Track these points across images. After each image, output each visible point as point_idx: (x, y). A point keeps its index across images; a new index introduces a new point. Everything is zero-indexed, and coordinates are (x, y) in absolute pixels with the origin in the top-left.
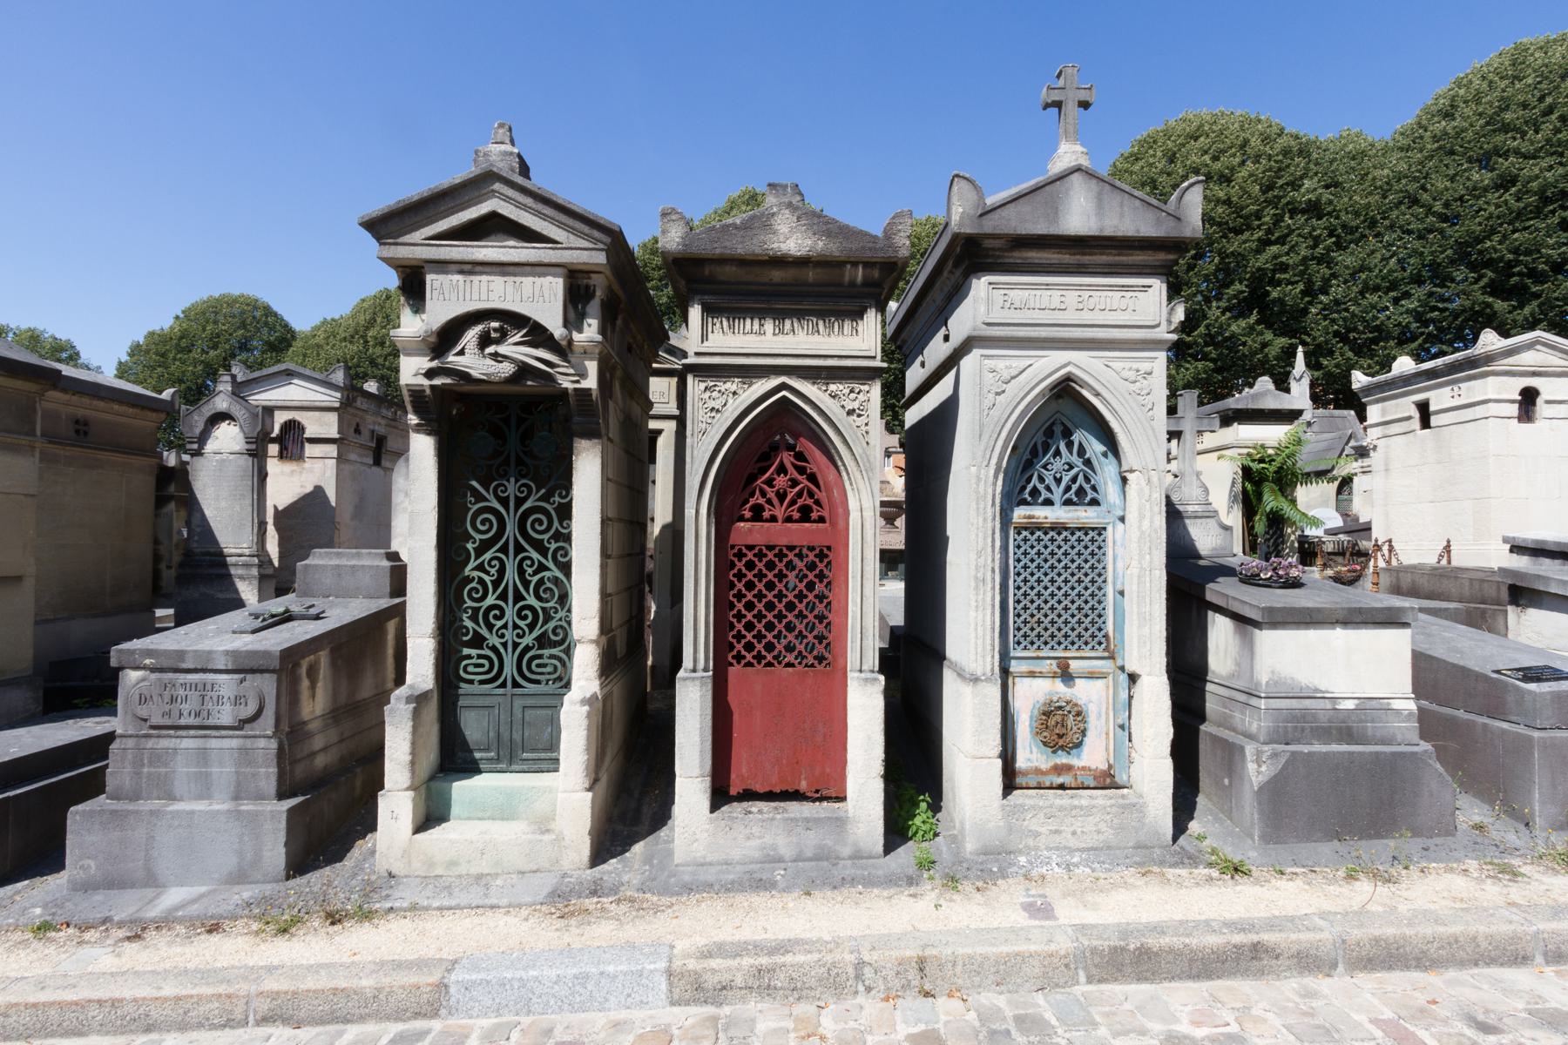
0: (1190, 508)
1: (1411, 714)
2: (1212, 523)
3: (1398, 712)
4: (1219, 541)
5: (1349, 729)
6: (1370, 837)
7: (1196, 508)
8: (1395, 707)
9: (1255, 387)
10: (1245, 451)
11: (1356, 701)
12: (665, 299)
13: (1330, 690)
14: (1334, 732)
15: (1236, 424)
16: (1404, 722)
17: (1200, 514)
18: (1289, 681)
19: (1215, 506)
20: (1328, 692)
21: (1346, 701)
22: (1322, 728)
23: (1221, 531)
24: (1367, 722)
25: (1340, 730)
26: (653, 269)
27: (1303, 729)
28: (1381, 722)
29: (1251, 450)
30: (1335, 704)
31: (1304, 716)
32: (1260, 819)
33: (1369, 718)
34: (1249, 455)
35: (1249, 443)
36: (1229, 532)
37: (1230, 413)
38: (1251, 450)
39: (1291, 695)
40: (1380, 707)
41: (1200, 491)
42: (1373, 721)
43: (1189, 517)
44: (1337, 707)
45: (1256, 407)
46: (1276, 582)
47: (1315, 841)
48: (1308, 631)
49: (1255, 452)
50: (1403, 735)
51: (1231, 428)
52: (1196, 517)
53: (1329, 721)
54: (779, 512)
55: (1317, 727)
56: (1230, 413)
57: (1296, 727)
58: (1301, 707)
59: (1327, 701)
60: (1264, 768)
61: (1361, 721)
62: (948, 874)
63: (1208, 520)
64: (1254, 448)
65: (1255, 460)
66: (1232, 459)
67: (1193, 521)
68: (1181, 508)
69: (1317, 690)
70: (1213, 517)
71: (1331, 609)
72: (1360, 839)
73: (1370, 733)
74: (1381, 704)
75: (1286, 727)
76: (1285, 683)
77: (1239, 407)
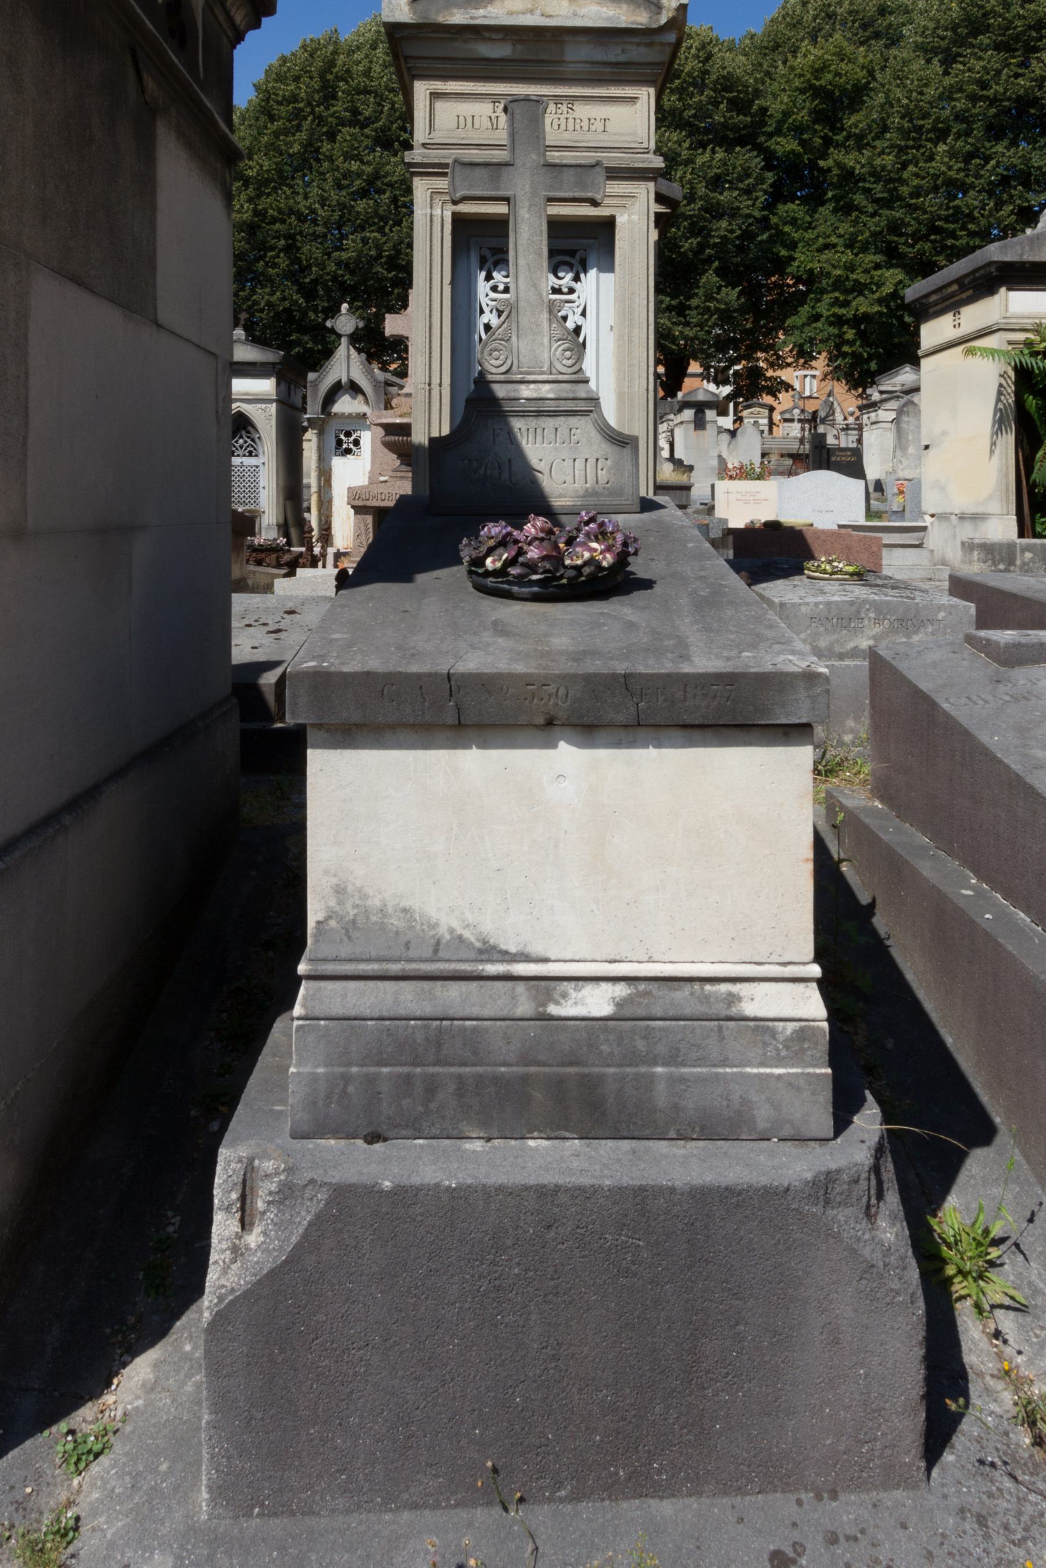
0: (526, 392)
1: (804, 1033)
2: (583, 426)
3: (762, 1026)
4: (603, 475)
5: (590, 1084)
6: (613, 1490)
7: (546, 391)
8: (749, 1009)
9: (1040, 225)
10: (1021, 336)
11: (621, 990)
12: (296, 148)
13: (536, 948)
14: (538, 1096)
15: (1003, 290)
16: (779, 1061)
17: (551, 406)
18: (396, 922)
19: (588, 374)
20: (527, 958)
21: (589, 990)
22: (497, 1080)
23: (604, 448)
24: (655, 1063)
25: (557, 1086)
26: (280, 103)
27: (431, 1087)
28: (700, 1062)
29: (1031, 336)
30: (549, 997)
31: (438, 1041)
32: (213, 1425)
33: (661, 1049)
34: (1028, 344)
35: (1028, 323)
36: (627, 451)
37: (993, 269)
38: (1031, 336)
39: (395, 968)
40: (700, 1009)
41: (559, 349)
42: (673, 1059)
43: (523, 414)
44: (553, 1010)
45: (1037, 259)
46: (520, 580)
47: (415, 1506)
48: (460, 753)
49: (1038, 338)
50: (777, 1107)
51: (996, 297)
52: (539, 414)
53: (526, 1059)
54: (241, 452)
55: (480, 1079)
56: (993, 269)
57: (408, 1079)
58: (428, 1009)
59: (521, 987)
60: (253, 1239)
61: (633, 1058)
62: (678, 1050)
63: (573, 421)
64: (1037, 331)
65: (1037, 353)
66: (992, 352)
67: (532, 422)
68: (500, 391)
69: (489, 952)
70: (586, 413)
71: (527, 680)
72: (576, 1497)
73: (661, 1097)
74: (706, 998)
75: (371, 1080)
76: (382, 927)
77: (1008, 258)
